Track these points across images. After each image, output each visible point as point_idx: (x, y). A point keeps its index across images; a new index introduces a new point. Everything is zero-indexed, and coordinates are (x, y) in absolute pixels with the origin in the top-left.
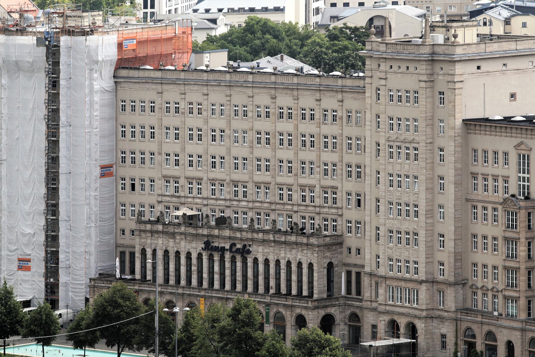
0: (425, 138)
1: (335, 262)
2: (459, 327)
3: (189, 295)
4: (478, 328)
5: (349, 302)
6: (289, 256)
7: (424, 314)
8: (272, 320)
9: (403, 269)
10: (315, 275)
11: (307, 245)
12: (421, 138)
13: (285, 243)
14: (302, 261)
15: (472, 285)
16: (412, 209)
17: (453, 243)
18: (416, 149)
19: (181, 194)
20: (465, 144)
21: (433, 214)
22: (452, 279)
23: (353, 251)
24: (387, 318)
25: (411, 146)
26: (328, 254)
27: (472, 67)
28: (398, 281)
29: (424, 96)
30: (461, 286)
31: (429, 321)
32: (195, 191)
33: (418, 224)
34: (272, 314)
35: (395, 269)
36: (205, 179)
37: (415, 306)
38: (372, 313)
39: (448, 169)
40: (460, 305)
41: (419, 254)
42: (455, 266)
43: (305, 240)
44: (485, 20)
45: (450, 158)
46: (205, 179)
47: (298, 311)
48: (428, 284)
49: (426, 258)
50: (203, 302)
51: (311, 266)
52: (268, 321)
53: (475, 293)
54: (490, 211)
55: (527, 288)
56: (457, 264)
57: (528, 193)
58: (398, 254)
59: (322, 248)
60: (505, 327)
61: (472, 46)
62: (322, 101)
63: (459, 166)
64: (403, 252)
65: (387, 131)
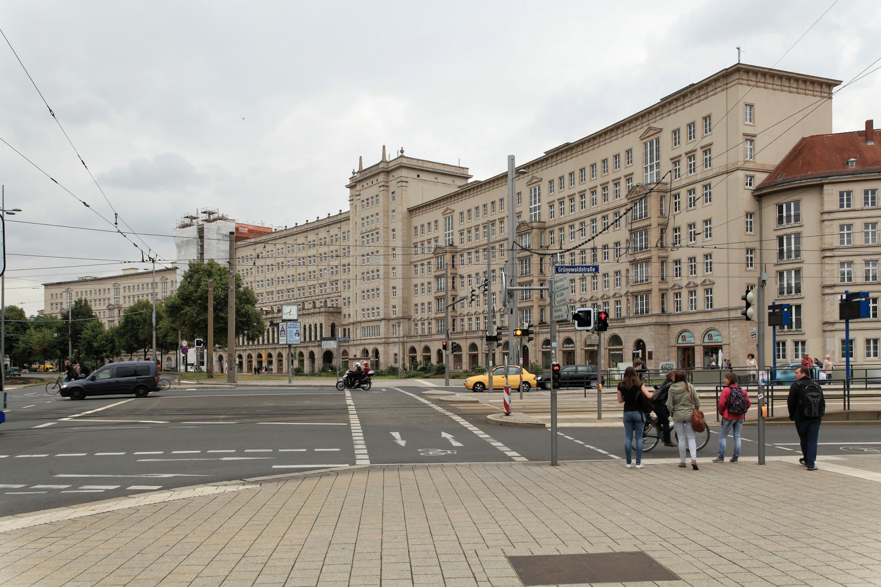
1: (336, 324)
7: (383, 340)
12: (380, 225)
16: (375, 274)
18: (377, 233)
22: (401, 315)
24: (361, 348)
27: (414, 174)
33: (380, 283)
39: (398, 242)
40: (407, 333)
41: (380, 302)
44: (569, 347)
47: (310, 349)
53: (416, 325)
54: (426, 267)
60: (436, 340)
64: (370, 303)
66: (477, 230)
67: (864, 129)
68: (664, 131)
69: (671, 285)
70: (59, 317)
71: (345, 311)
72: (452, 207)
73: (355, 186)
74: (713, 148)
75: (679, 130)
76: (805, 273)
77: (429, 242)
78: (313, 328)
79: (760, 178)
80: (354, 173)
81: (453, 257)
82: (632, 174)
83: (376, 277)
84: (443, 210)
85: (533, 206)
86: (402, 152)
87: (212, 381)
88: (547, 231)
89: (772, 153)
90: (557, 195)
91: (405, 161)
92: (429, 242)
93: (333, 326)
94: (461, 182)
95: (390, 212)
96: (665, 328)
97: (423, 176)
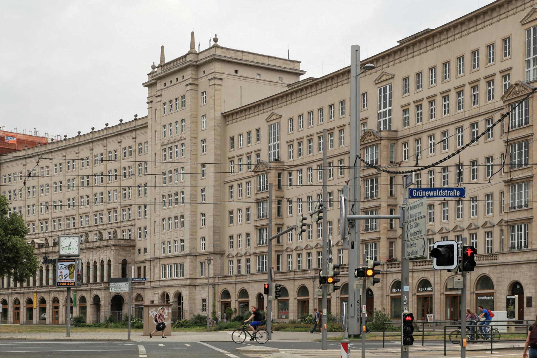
0: (190, 133)
2: (216, 291)
3: (28, 293)
4: (233, 288)
5: (136, 286)
6: (95, 257)
8: (78, 303)
9: (173, 249)
10: (112, 268)
11: (107, 246)
13: (93, 248)
14: (103, 259)
15: (229, 255)
16: (179, 197)
17: (213, 218)
19: (37, 232)
20: (222, 135)
21: (196, 198)
22: (211, 250)
23: (142, 251)
24: (160, 291)
25: (179, 144)
26: (123, 253)
27: (230, 69)
28: (169, 259)
29: (190, 97)
30: (219, 256)
31: (192, 288)
32: (44, 229)
34: (78, 298)
35: (167, 250)
36: (50, 219)
37: (182, 277)
38: (151, 291)
40: (218, 272)
41: (185, 233)
42: (214, 238)
43: (105, 243)
45: (210, 145)
46: (50, 219)
47: (95, 292)
48: (192, 257)
49: (191, 235)
50: (35, 297)
51: (109, 261)
52: (75, 305)
53: (231, 262)
55: (276, 243)
56: (216, 237)
57: (279, 157)
58: (169, 237)
59: (118, 248)
61: (231, 51)
62: (122, 143)
63: (219, 152)
65: (161, 138)
84: (522, 15)
86: (216, 40)
88: (400, 142)
90: (413, 96)
94: (289, 80)
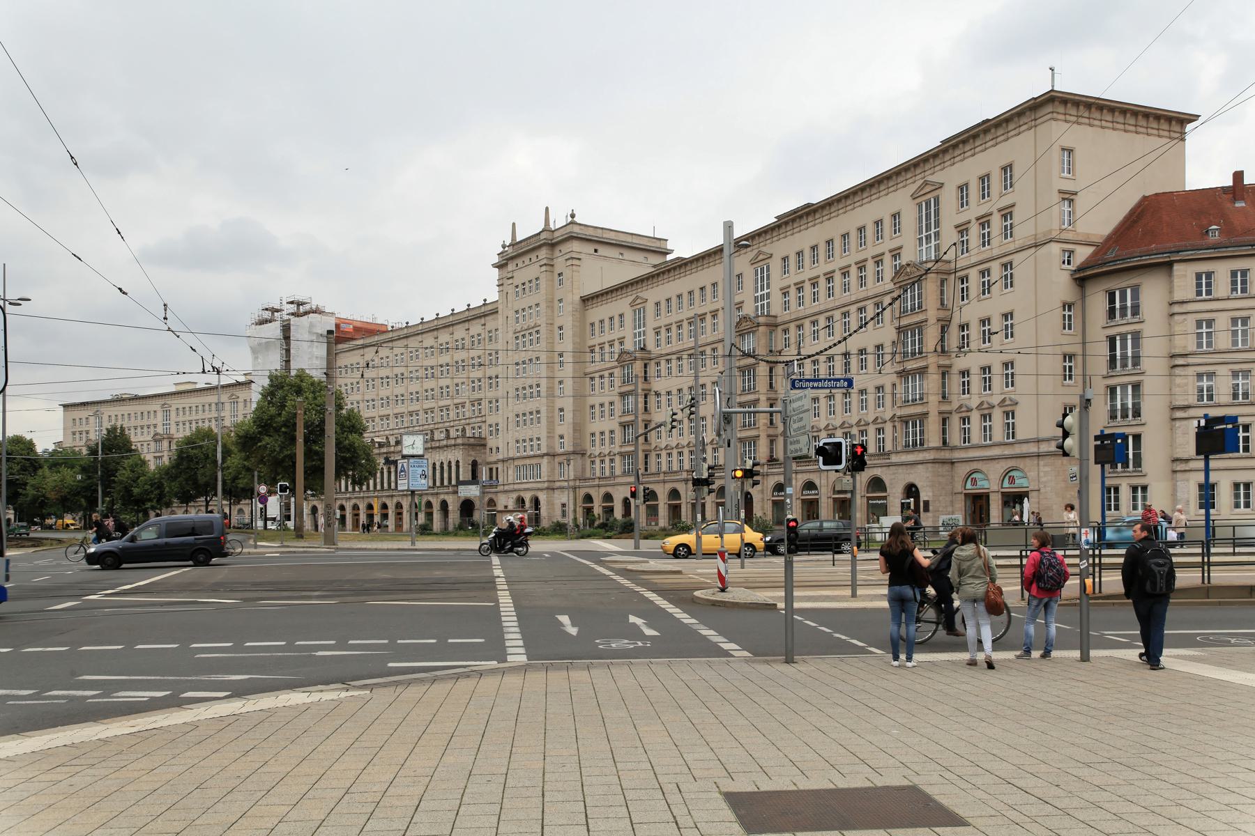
1: (479, 461)
7: (546, 485)
12: (542, 321)
16: (535, 390)
18: (537, 332)
21: (367, 528)
22: (571, 449)
24: (515, 495)
27: (589, 248)
33: (541, 404)
39: (567, 345)
40: (579, 474)
41: (541, 430)
47: (442, 497)
53: (593, 462)
54: (606, 380)
60: (622, 484)
64: (526, 432)
66: (679, 327)
67: (1231, 184)
68: (945, 187)
69: (955, 405)
70: (85, 451)
71: (491, 443)
72: (644, 295)
73: (506, 264)
74: (1016, 211)
75: (967, 185)
76: (1146, 389)
77: (611, 344)
78: (446, 467)
79: (1083, 254)
80: (504, 246)
81: (646, 366)
82: (900, 248)
83: (535, 394)
84: (630, 299)
85: (760, 293)
86: (573, 216)
87: (302, 543)
88: (780, 329)
89: (1100, 218)
90: (793, 277)
91: (576, 229)
92: (611, 344)
93: (474, 465)
94: (656, 260)
95: (556, 302)
96: (947, 467)
97: (603, 251)
